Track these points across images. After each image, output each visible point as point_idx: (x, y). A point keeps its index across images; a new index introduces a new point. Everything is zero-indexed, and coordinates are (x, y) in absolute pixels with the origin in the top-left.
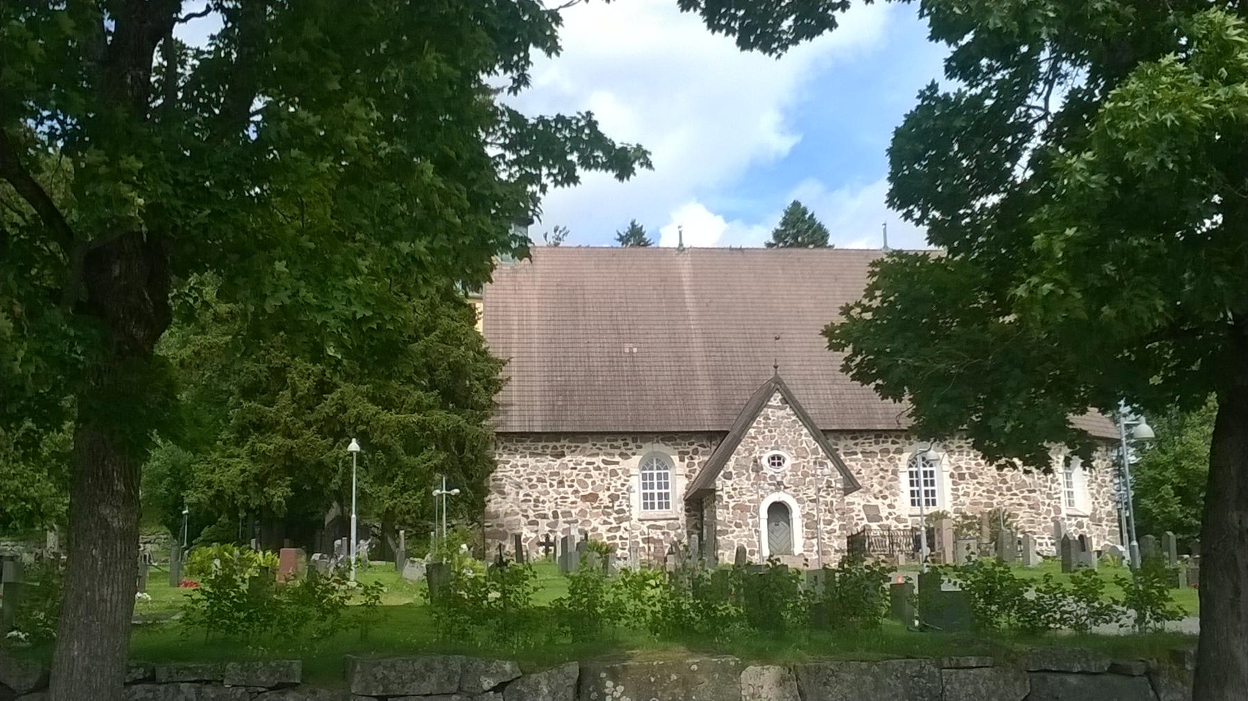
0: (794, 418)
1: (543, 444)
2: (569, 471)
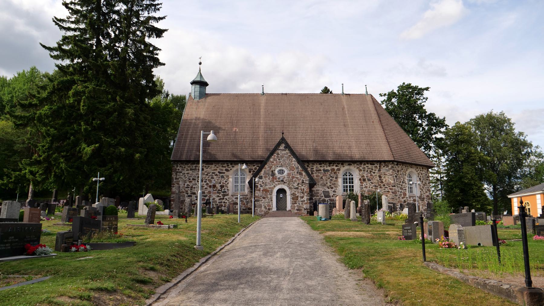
0: (289, 154)
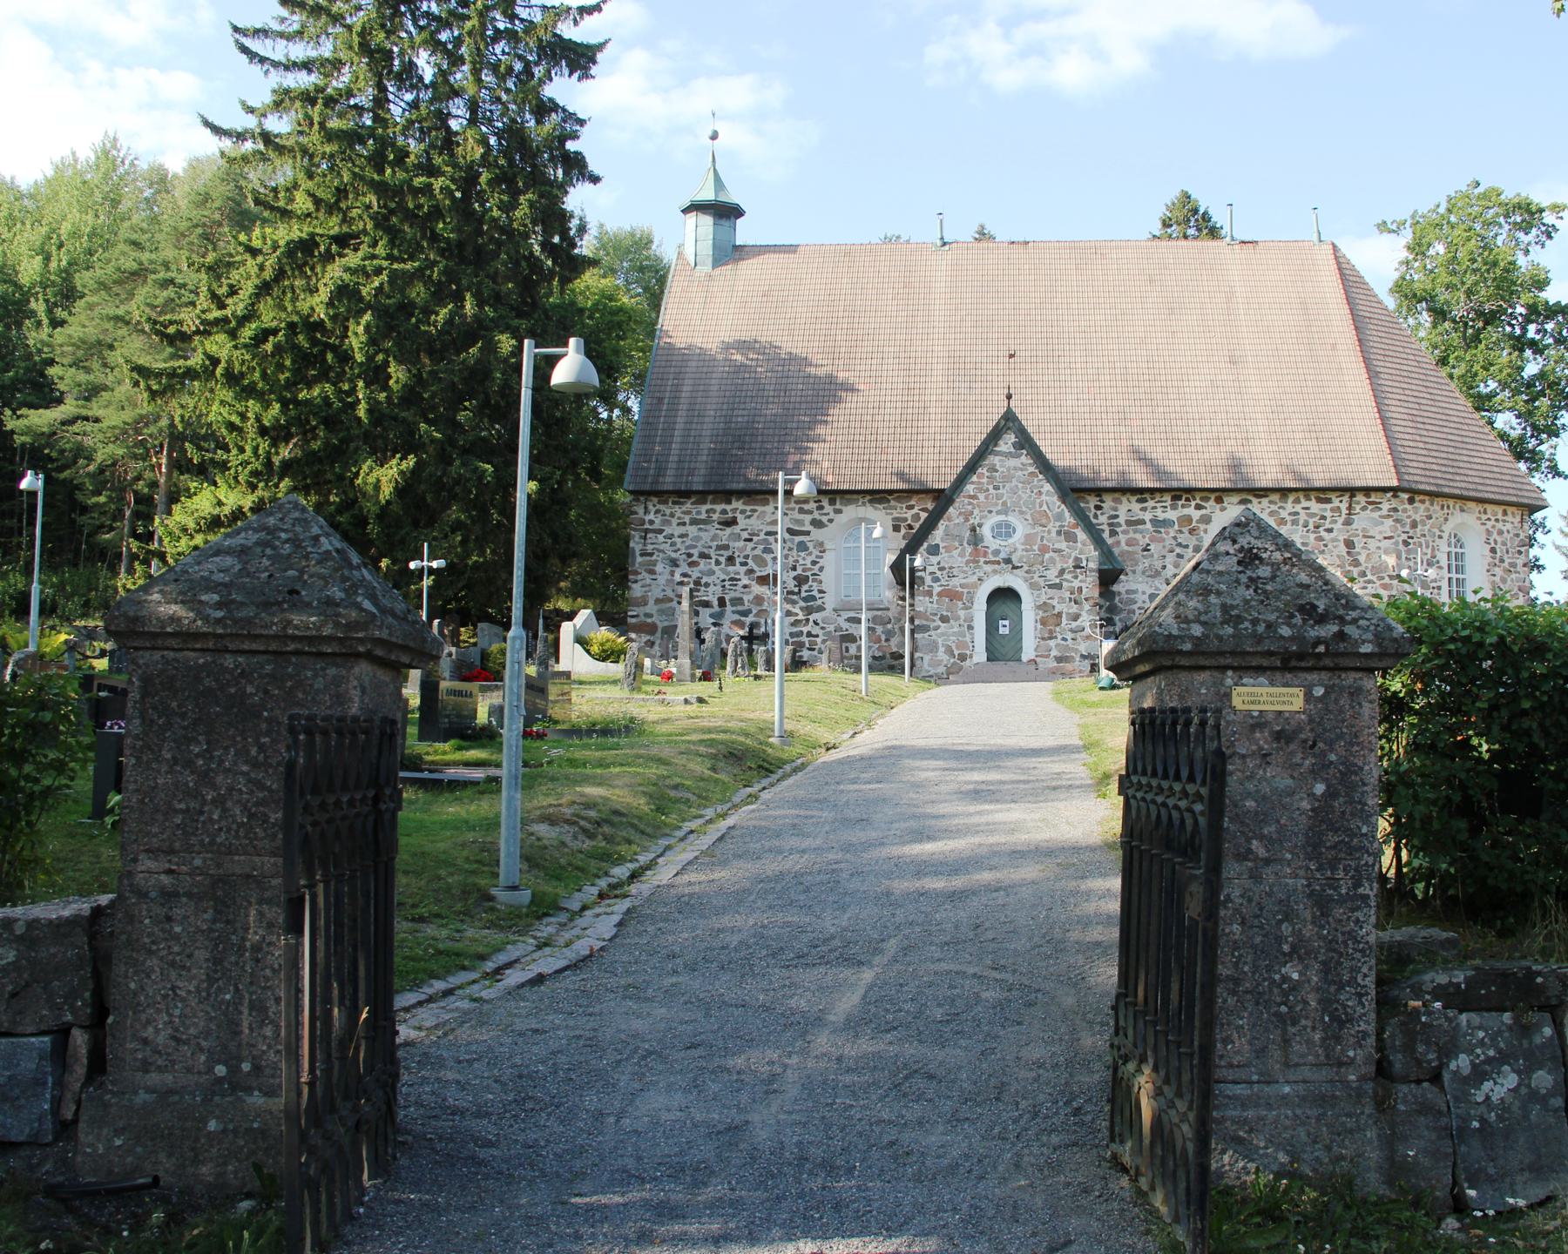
0: (1032, 469)
1: (708, 506)
2: (742, 543)
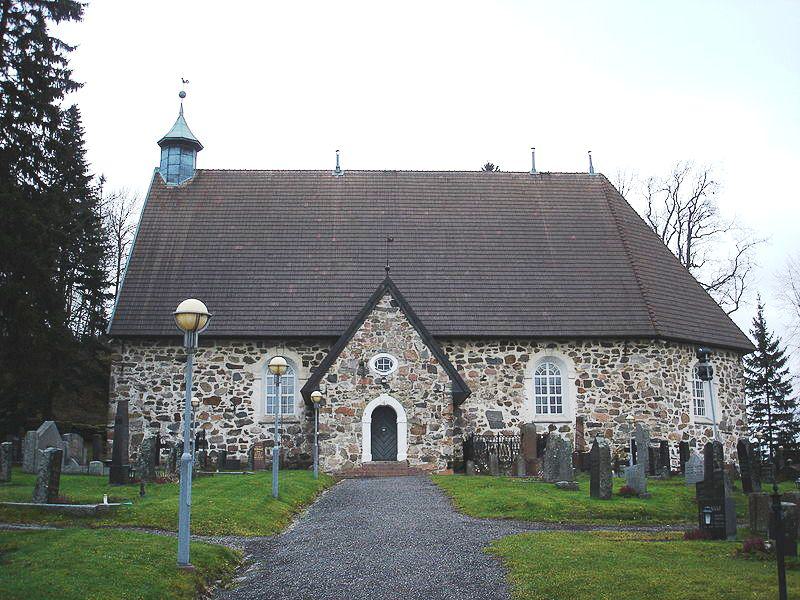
0: (404, 321)
